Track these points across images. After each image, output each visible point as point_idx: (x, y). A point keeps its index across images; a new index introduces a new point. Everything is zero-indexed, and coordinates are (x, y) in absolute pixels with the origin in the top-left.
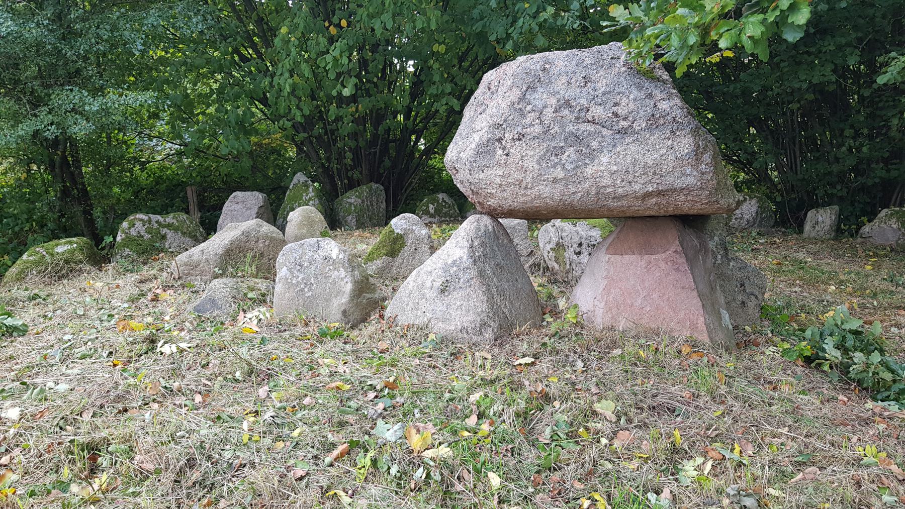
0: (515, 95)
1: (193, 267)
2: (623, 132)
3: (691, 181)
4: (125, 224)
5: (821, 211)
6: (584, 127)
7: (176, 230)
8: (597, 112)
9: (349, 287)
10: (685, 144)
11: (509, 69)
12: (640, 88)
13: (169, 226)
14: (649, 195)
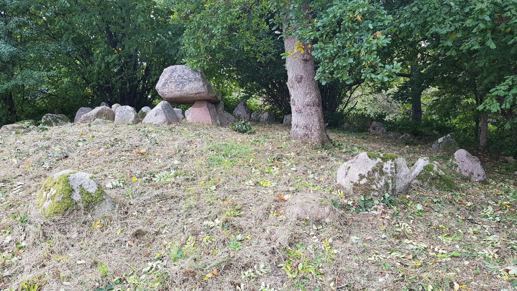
0: (169, 74)
1: (88, 118)
2: (190, 81)
3: (203, 91)
4: (45, 117)
5: (288, 115)
6: (183, 80)
7: (62, 120)
8: (185, 77)
9: (134, 116)
10: (201, 83)
11: (169, 68)
12: (193, 73)
13: (59, 118)
14: (196, 94)
